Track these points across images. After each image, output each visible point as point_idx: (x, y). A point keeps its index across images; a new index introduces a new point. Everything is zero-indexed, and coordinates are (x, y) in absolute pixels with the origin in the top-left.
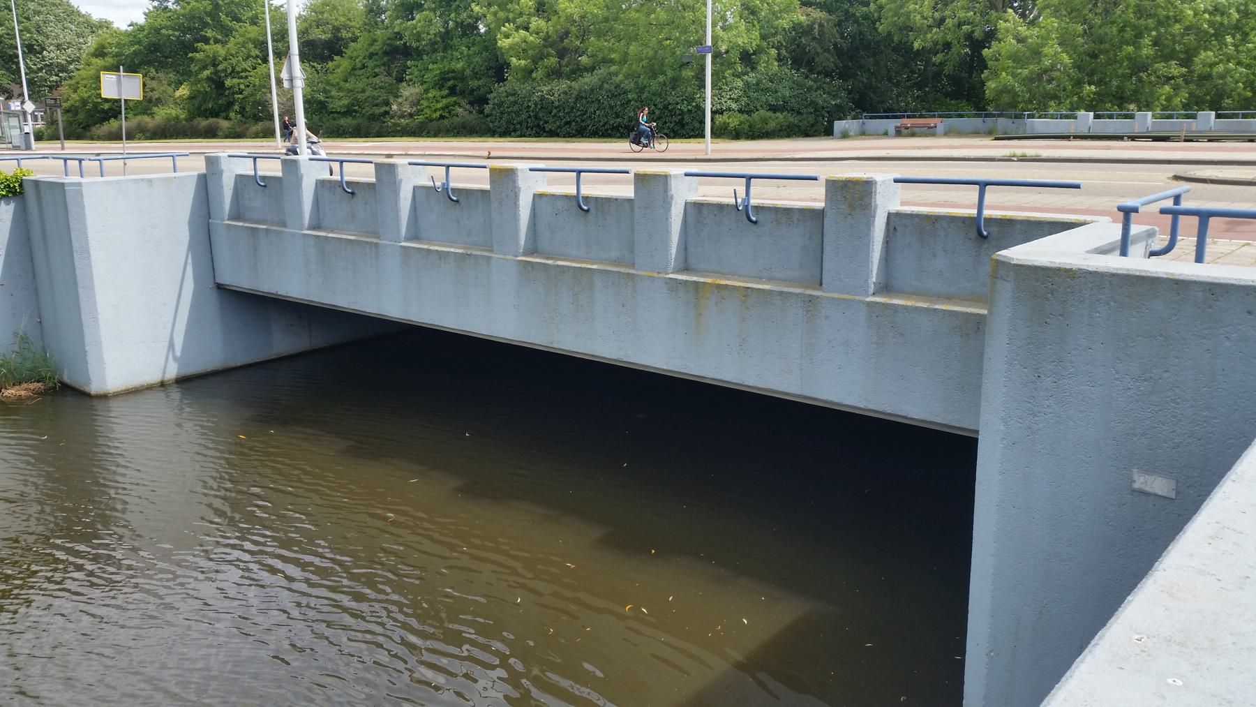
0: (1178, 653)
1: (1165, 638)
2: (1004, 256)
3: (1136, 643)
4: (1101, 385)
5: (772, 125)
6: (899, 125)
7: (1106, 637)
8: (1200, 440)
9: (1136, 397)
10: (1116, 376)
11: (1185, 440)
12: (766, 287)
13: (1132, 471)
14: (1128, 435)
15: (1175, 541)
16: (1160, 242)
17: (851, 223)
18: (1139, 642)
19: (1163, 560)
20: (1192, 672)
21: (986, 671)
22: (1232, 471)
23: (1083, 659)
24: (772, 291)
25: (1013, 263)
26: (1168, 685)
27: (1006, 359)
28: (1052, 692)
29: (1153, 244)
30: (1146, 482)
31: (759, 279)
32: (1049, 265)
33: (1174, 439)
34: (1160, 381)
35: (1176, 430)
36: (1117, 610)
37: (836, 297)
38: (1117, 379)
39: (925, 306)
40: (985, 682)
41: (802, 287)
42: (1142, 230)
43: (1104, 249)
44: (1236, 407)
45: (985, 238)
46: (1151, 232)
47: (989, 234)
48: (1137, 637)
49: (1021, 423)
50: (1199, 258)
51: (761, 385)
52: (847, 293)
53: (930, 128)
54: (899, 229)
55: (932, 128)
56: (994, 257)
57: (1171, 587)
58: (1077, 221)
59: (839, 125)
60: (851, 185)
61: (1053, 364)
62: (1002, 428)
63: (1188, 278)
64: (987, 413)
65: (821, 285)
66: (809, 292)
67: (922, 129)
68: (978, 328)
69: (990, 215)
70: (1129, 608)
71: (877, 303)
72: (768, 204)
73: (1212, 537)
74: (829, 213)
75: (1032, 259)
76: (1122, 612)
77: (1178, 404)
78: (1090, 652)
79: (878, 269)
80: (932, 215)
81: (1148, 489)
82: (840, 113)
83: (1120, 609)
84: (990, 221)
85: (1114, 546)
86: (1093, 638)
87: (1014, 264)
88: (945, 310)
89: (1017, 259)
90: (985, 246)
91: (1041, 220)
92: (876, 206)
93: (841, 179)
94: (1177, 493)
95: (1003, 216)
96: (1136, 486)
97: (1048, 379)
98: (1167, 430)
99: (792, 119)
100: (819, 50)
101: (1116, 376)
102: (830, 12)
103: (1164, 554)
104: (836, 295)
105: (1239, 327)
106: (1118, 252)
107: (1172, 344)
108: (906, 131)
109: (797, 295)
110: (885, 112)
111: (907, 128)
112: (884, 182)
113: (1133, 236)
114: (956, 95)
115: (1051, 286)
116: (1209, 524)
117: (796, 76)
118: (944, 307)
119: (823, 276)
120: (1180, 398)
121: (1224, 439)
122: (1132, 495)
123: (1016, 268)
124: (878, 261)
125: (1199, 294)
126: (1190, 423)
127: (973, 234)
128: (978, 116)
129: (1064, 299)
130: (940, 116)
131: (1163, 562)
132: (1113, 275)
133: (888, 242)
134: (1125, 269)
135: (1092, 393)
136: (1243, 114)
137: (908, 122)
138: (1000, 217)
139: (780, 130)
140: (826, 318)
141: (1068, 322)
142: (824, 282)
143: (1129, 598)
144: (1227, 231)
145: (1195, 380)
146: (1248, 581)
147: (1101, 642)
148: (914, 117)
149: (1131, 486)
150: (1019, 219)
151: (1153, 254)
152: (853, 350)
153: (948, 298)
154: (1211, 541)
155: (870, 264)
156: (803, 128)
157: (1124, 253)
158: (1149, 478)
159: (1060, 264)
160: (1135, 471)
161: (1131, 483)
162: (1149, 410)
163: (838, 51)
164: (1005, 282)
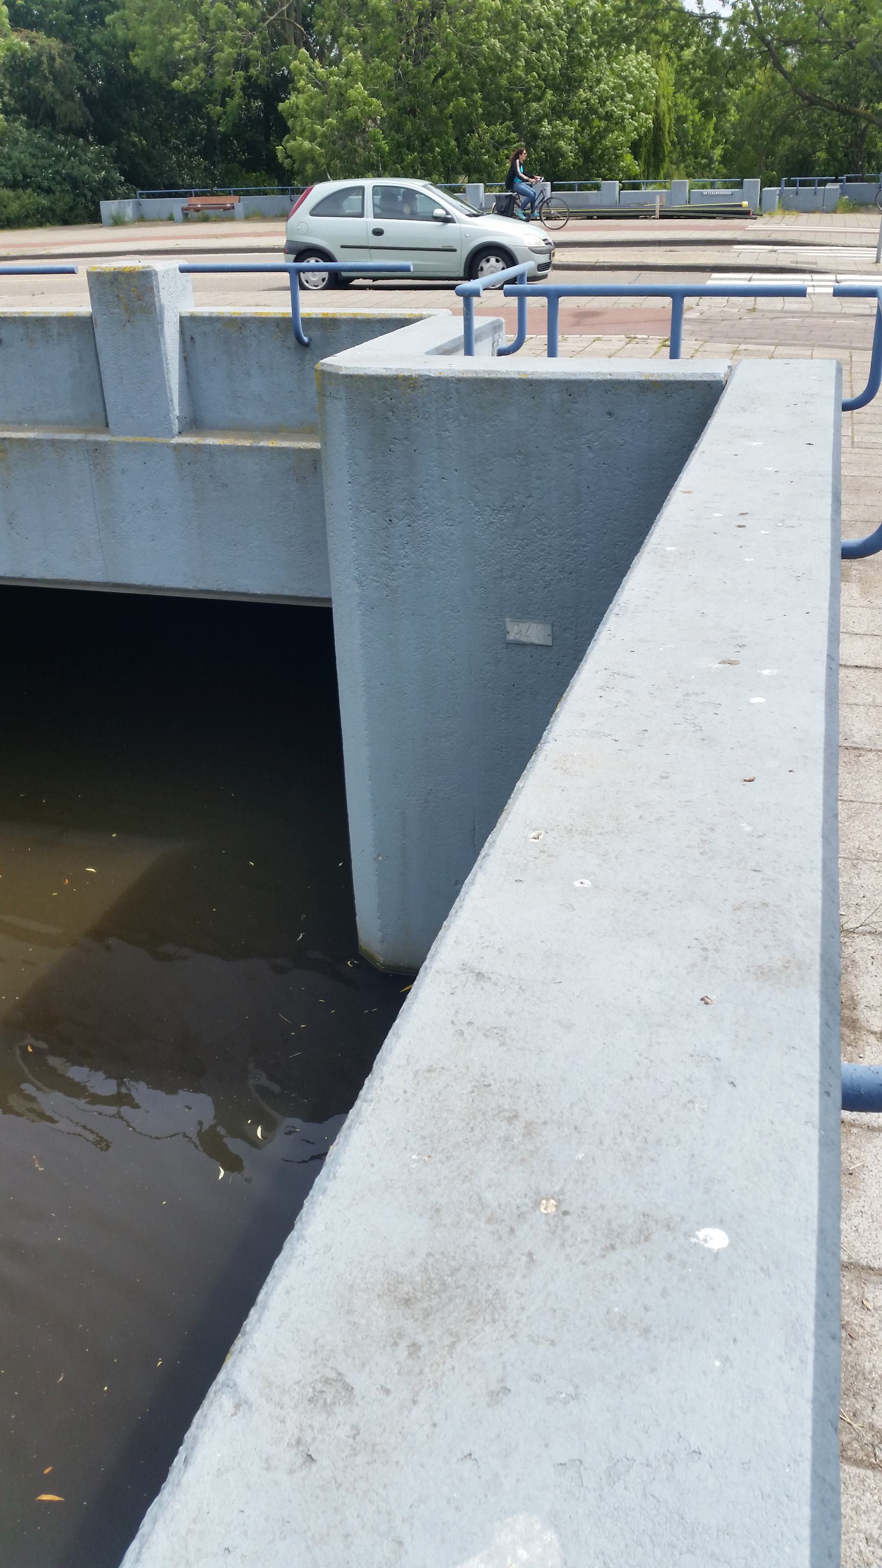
0: (581, 845)
1: (566, 828)
2: (330, 365)
3: (534, 843)
4: (461, 523)
5: (14, 208)
6: (186, 205)
7: (498, 842)
8: (571, 573)
9: (500, 532)
10: (476, 509)
11: (555, 576)
12: (31, 435)
13: (504, 621)
14: (495, 578)
15: (562, 700)
16: (507, 339)
17: (132, 335)
18: (537, 841)
19: (551, 728)
20: (599, 865)
21: (376, 878)
22: (614, 602)
23: (473, 879)
24: (40, 440)
25: (342, 373)
26: (576, 889)
27: (350, 503)
28: (440, 933)
29: (500, 340)
30: (521, 631)
31: (19, 424)
32: (383, 372)
33: (545, 576)
34: (524, 509)
35: (546, 566)
36: (506, 803)
37: (131, 441)
38: (477, 513)
39: (248, 445)
40: (376, 891)
41: (81, 431)
42: (487, 322)
43: (445, 348)
44: (605, 530)
45: (307, 345)
46: (497, 324)
47: (310, 339)
48: (534, 834)
49: (377, 582)
50: (552, 352)
51: (48, 576)
52: (145, 435)
53: (225, 209)
54: (198, 339)
55: (228, 209)
56: (318, 366)
57: (565, 761)
58: (412, 317)
59: (108, 207)
60: (122, 278)
61: (404, 503)
62: (357, 590)
63: (544, 377)
64: (337, 575)
65: (107, 426)
66: (92, 437)
67: (217, 211)
68: (315, 468)
69: (309, 314)
70: (521, 797)
71: (186, 445)
72: (11, 313)
73: (602, 688)
74: (99, 320)
75: (364, 366)
76: (514, 804)
77: (544, 534)
78: (480, 867)
79: (180, 396)
80: (236, 318)
81: (524, 639)
82: (107, 191)
83: (510, 801)
84: (310, 322)
85: (495, 710)
86: (482, 847)
87: (343, 375)
88: (272, 448)
89: (346, 368)
90: (308, 357)
91: (370, 317)
92: (162, 307)
93: (107, 270)
94: (554, 639)
95: (323, 314)
96: (511, 637)
97: (401, 523)
98: (537, 567)
99: (44, 201)
100: (58, 96)
101: (476, 509)
102: (65, 39)
103: (552, 719)
104: (130, 439)
105: (601, 433)
106: (463, 351)
107: (532, 463)
108: (196, 214)
109: (77, 442)
110: (166, 188)
111: (197, 210)
112: (167, 272)
113: (476, 330)
114: (251, 166)
115: (389, 401)
116: (597, 672)
117: (38, 138)
118: (269, 444)
119: (108, 414)
120: (546, 527)
121: (595, 569)
122: (507, 648)
123: (346, 380)
124: (177, 386)
125: (556, 396)
126: (559, 556)
127: (292, 341)
128: (283, 192)
129: (407, 417)
130: (236, 193)
131: (552, 730)
132: (459, 380)
133: (186, 359)
134: (472, 371)
135: (452, 534)
136: (579, 185)
137: (198, 202)
138: (321, 316)
139: (27, 216)
140: (123, 471)
141: (415, 448)
142: (110, 420)
143: (519, 784)
144: (577, 324)
145: (560, 503)
146: (647, 734)
147: (492, 851)
148: (204, 194)
149: (505, 637)
150: (344, 317)
151: (501, 353)
152: (166, 514)
153: (274, 432)
154: (602, 693)
155: (168, 390)
156: (58, 212)
157: (469, 352)
158: (524, 626)
159: (397, 370)
160: (508, 619)
161: (505, 634)
162: (515, 547)
163: (88, 100)
164: (336, 401)
